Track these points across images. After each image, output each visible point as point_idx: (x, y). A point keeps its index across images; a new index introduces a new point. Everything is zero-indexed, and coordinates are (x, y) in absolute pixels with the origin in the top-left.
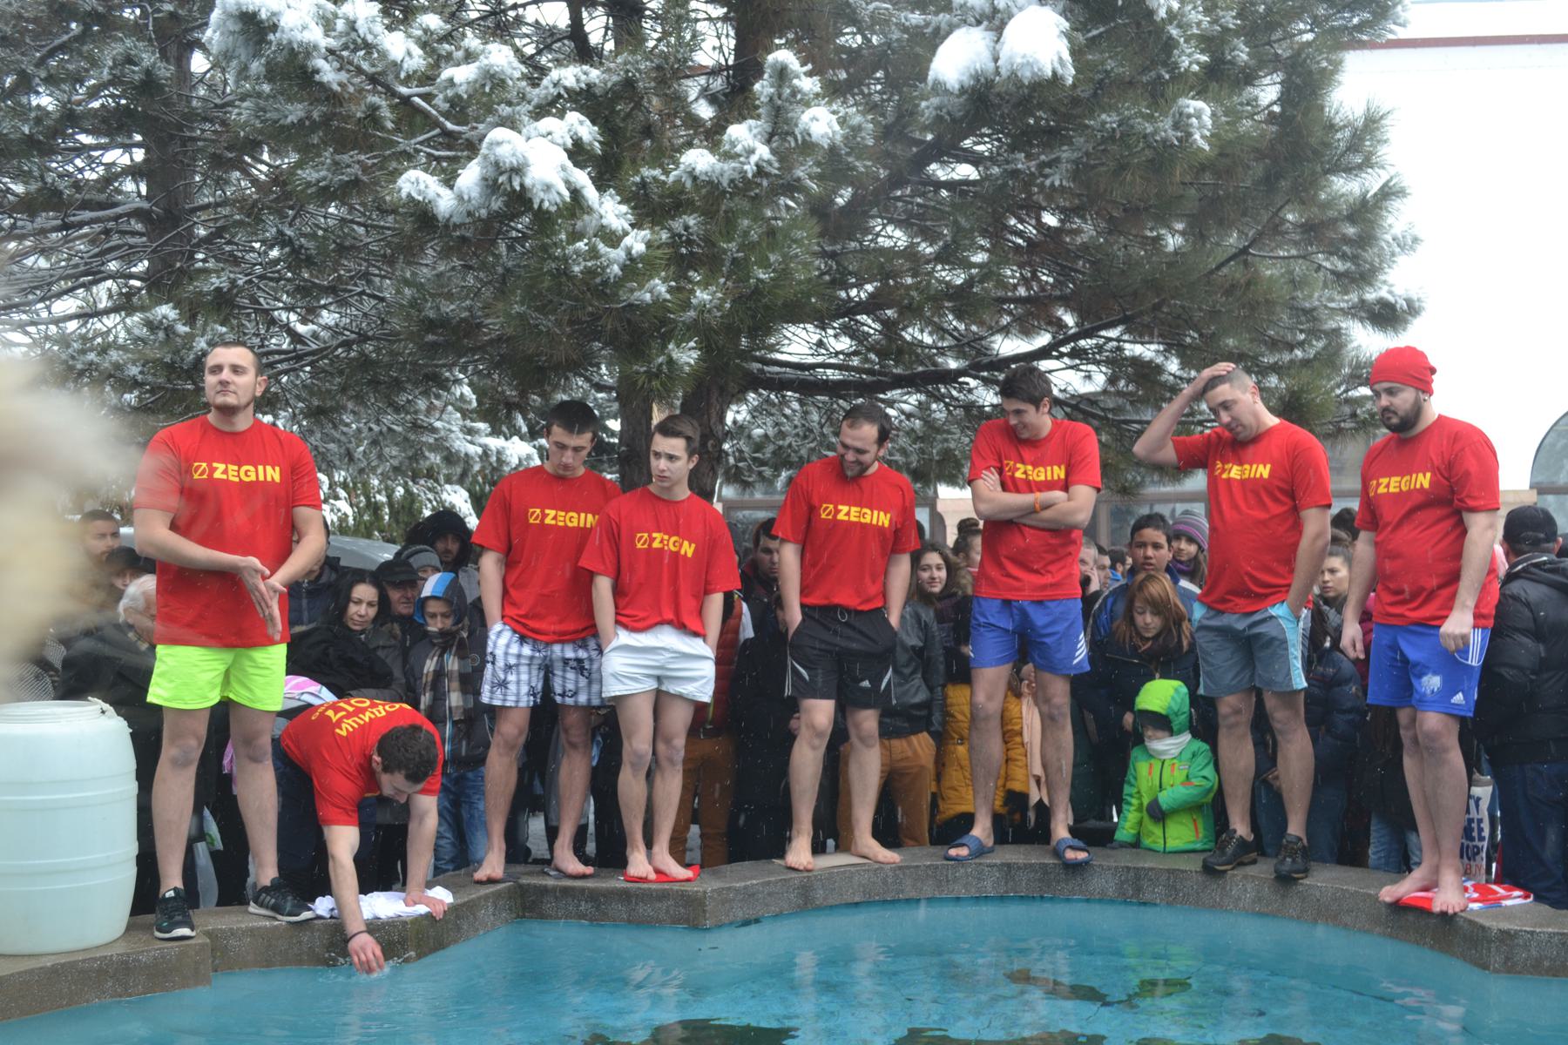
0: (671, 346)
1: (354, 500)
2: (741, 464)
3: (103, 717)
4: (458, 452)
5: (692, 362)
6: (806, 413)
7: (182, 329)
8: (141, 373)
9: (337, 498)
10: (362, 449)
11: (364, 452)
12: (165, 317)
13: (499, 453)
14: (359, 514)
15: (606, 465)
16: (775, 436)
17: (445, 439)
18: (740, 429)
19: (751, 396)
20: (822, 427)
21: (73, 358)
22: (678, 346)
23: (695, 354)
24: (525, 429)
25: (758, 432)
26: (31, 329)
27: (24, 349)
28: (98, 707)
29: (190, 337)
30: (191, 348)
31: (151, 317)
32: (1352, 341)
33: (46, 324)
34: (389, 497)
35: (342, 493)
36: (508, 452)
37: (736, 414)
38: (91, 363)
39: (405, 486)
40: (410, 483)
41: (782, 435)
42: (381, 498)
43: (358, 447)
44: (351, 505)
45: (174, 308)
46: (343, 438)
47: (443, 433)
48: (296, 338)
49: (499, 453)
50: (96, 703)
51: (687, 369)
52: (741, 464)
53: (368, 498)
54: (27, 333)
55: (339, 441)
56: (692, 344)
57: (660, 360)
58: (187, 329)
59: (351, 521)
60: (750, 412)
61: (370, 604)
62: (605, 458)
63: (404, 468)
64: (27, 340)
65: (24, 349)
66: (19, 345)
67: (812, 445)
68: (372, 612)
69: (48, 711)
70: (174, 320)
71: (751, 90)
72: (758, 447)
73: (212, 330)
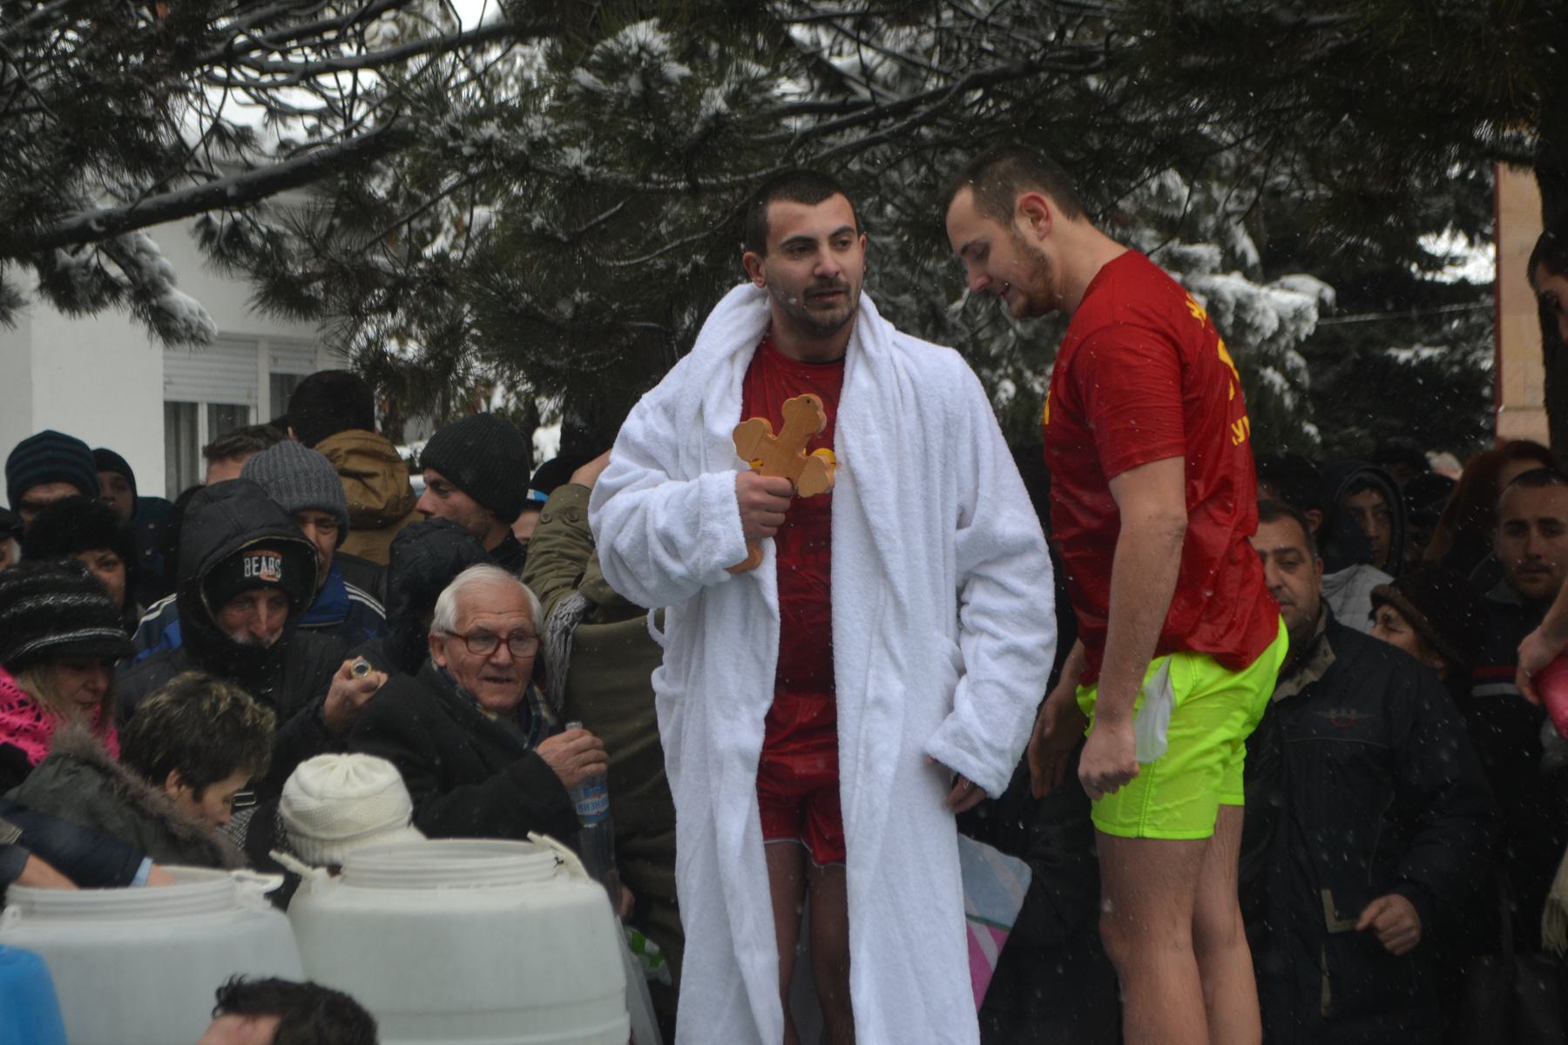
7: (676, 70)
8: (589, 161)
10: (959, 304)
11: (964, 310)
12: (643, 47)
13: (1242, 306)
15: (1419, 330)
21: (454, 134)
24: (1253, 257)
26: (327, 80)
27: (371, 116)
28: (550, 855)
31: (617, 49)
32: (393, 33)
33: (354, 68)
36: (1259, 305)
38: (489, 143)
39: (1018, 379)
40: (1028, 374)
43: (952, 301)
45: (661, 28)
46: (925, 284)
48: (832, 79)
49: (1242, 306)
50: (544, 847)
54: (316, 89)
58: (685, 70)
62: (1415, 313)
63: (1043, 342)
64: (317, 103)
65: (310, 121)
66: (302, 113)
70: (663, 54)
73: (739, 71)
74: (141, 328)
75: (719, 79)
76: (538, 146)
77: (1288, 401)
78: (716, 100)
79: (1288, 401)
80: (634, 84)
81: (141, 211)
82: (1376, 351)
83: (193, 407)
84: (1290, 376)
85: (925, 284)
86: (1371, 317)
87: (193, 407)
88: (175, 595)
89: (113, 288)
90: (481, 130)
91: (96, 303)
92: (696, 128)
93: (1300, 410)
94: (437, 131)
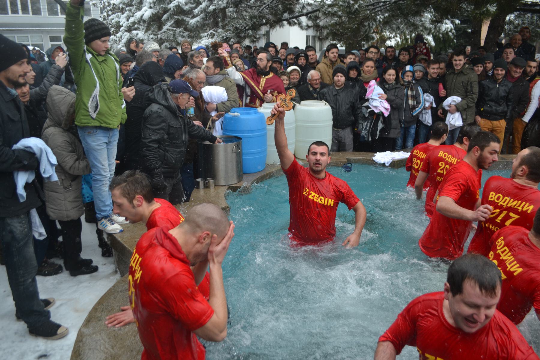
0: (488, 6)
1: (401, 37)
2: (510, 32)
3: (326, 106)
4: (428, 27)
5: (494, 10)
6: (533, 17)
9: (397, 37)
14: (402, 42)
16: (522, 24)
17: (424, 23)
18: (511, 22)
19: (515, 13)
20: (537, 21)
22: (490, 5)
23: (495, 8)
25: (517, 22)
29: (353, 5)
30: (354, 7)
34: (411, 36)
35: (398, 36)
37: (510, 17)
38: (330, 11)
41: (524, 23)
42: (408, 37)
44: (400, 39)
46: (397, 24)
47: (424, 22)
51: (492, 12)
52: (510, 32)
53: (405, 37)
55: (396, 24)
56: (495, 5)
57: (484, 9)
59: (400, 43)
60: (515, 16)
61: (393, 75)
67: (533, 27)
68: (394, 77)
69: (315, 104)
71: (489, 143)
72: (516, 27)
74: (299, 28)
75: (357, 4)
76: (335, 12)
77: (452, 37)
78: (356, 6)
79: (452, 37)
80: (346, 4)
81: (102, 235)
82: (466, 30)
83: (309, 36)
84: (453, 34)
85: (397, 24)
86: (465, 25)
87: (309, 36)
88: (257, 100)
89: (296, 23)
90: (108, 222)
91: (294, 25)
92: (354, 10)
93: (454, 38)
94: (323, 10)
